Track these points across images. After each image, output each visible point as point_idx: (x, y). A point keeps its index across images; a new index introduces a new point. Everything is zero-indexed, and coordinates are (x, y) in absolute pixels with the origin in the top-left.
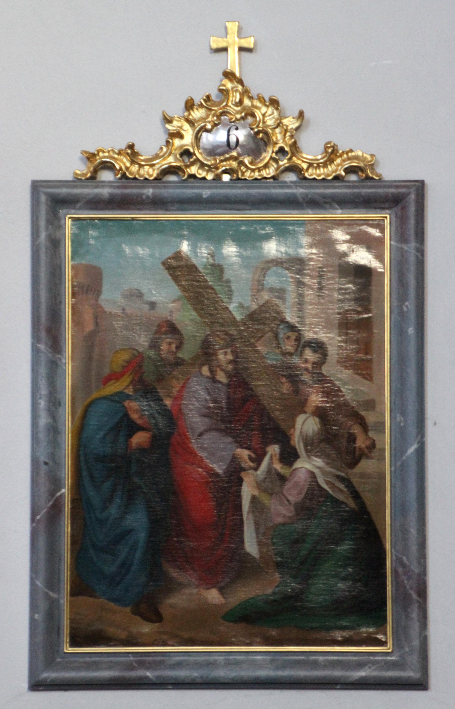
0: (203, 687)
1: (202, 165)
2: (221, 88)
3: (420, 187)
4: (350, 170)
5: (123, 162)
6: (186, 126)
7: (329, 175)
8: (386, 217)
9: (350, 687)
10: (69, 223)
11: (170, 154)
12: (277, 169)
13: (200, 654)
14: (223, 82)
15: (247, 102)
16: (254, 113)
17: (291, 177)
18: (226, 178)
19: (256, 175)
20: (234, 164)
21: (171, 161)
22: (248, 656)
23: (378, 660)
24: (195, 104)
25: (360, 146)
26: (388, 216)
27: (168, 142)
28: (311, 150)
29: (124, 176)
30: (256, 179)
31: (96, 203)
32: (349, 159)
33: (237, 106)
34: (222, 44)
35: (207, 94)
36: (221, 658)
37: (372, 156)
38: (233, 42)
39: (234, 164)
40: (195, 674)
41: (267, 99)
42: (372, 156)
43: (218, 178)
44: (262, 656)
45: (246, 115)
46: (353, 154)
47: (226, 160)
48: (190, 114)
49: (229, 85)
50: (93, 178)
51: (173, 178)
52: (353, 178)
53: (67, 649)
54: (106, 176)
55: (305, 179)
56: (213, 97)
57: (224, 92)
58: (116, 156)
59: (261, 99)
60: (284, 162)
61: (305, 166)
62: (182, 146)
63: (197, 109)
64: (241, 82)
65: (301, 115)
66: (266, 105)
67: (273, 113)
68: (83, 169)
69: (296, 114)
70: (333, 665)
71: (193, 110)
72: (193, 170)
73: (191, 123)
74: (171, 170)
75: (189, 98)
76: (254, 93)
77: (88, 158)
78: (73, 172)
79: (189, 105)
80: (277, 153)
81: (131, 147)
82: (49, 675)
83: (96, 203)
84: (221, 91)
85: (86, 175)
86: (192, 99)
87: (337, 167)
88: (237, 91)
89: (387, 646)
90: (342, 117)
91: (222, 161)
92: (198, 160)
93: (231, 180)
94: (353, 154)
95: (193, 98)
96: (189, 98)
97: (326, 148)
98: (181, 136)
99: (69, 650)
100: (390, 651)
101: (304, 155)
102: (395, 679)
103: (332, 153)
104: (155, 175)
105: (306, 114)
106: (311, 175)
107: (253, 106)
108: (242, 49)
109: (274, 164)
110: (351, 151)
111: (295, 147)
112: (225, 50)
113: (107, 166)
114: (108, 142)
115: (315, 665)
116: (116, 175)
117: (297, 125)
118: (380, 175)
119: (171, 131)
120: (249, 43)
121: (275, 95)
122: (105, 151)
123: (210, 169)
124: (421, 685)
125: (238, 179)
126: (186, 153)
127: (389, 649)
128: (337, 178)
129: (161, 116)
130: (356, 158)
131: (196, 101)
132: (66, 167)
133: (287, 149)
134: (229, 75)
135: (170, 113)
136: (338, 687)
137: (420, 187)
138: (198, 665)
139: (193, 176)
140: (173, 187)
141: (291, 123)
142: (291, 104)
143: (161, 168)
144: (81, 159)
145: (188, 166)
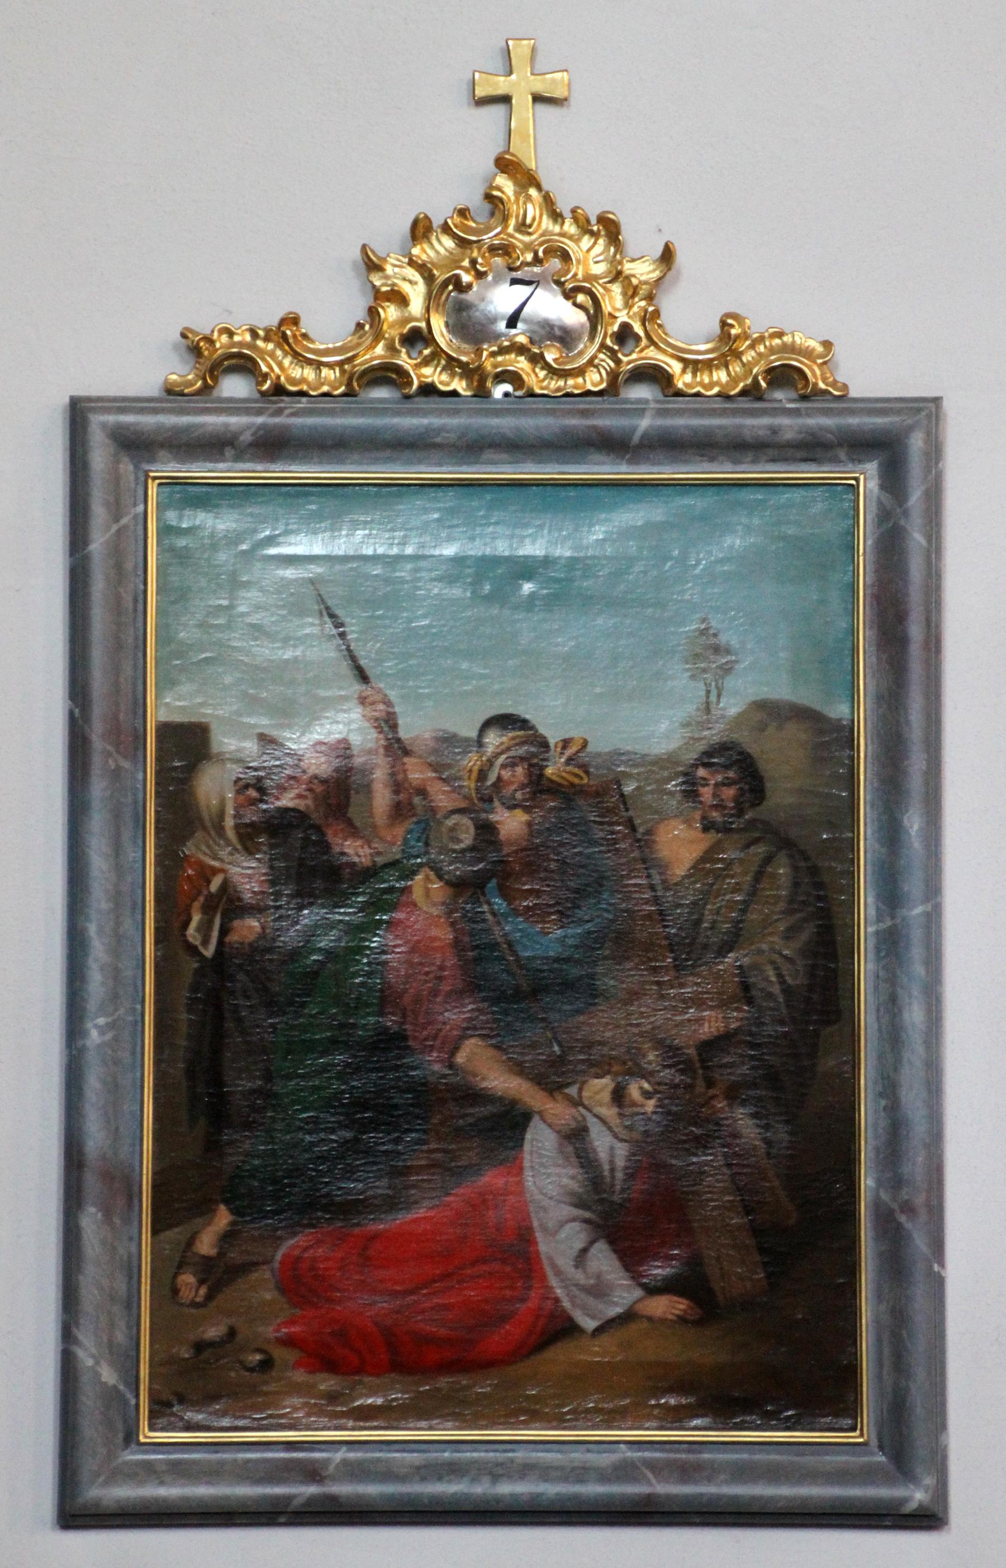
0: (632, 1520)
1: (452, 364)
2: (495, 193)
3: (928, 410)
4: (784, 376)
5: (282, 367)
8: (857, 479)
9: (730, 1519)
11: (378, 336)
13: (749, 1447)
17: (641, 392)
18: (499, 391)
20: (521, 364)
25: (793, 311)
27: (373, 312)
28: (688, 322)
29: (279, 390)
33: (530, 234)
34: (501, 85)
37: (827, 345)
38: (520, 85)
39: (521, 364)
40: (552, 1490)
41: (593, 220)
42: (827, 345)
43: (482, 393)
44: (779, 1453)
47: (502, 351)
49: (506, 186)
50: (206, 389)
51: (381, 393)
52: (779, 395)
53: (146, 1437)
54: (234, 387)
55: (679, 394)
57: (493, 201)
58: (260, 343)
59: (585, 228)
60: (631, 359)
61: (675, 367)
65: (667, 256)
66: (592, 233)
68: (180, 371)
70: (624, 1471)
72: (431, 374)
73: (423, 269)
74: (386, 374)
75: (422, 216)
76: (564, 206)
78: (161, 380)
79: (420, 230)
84: (489, 197)
85: (191, 384)
86: (426, 217)
90: (753, 257)
91: (493, 354)
92: (438, 353)
95: (430, 216)
97: (724, 324)
98: (401, 299)
100: (861, 1440)
102: (146, 1502)
103: (728, 341)
105: (682, 258)
110: (780, 335)
111: (649, 318)
112: (505, 99)
113: (243, 364)
114: (240, 311)
115: (313, 1473)
116: (261, 383)
117: (657, 274)
118: (845, 387)
120: (555, 83)
124: (929, 1519)
125: (532, 394)
126: (416, 338)
128: (752, 392)
129: (357, 254)
130: (792, 349)
132: (139, 366)
133: (638, 328)
134: (505, 164)
135: (379, 247)
136: (282, 1520)
137: (928, 410)
139: (428, 390)
140: (381, 410)
141: (643, 271)
143: (521, 372)
144: (176, 347)
145: (418, 366)
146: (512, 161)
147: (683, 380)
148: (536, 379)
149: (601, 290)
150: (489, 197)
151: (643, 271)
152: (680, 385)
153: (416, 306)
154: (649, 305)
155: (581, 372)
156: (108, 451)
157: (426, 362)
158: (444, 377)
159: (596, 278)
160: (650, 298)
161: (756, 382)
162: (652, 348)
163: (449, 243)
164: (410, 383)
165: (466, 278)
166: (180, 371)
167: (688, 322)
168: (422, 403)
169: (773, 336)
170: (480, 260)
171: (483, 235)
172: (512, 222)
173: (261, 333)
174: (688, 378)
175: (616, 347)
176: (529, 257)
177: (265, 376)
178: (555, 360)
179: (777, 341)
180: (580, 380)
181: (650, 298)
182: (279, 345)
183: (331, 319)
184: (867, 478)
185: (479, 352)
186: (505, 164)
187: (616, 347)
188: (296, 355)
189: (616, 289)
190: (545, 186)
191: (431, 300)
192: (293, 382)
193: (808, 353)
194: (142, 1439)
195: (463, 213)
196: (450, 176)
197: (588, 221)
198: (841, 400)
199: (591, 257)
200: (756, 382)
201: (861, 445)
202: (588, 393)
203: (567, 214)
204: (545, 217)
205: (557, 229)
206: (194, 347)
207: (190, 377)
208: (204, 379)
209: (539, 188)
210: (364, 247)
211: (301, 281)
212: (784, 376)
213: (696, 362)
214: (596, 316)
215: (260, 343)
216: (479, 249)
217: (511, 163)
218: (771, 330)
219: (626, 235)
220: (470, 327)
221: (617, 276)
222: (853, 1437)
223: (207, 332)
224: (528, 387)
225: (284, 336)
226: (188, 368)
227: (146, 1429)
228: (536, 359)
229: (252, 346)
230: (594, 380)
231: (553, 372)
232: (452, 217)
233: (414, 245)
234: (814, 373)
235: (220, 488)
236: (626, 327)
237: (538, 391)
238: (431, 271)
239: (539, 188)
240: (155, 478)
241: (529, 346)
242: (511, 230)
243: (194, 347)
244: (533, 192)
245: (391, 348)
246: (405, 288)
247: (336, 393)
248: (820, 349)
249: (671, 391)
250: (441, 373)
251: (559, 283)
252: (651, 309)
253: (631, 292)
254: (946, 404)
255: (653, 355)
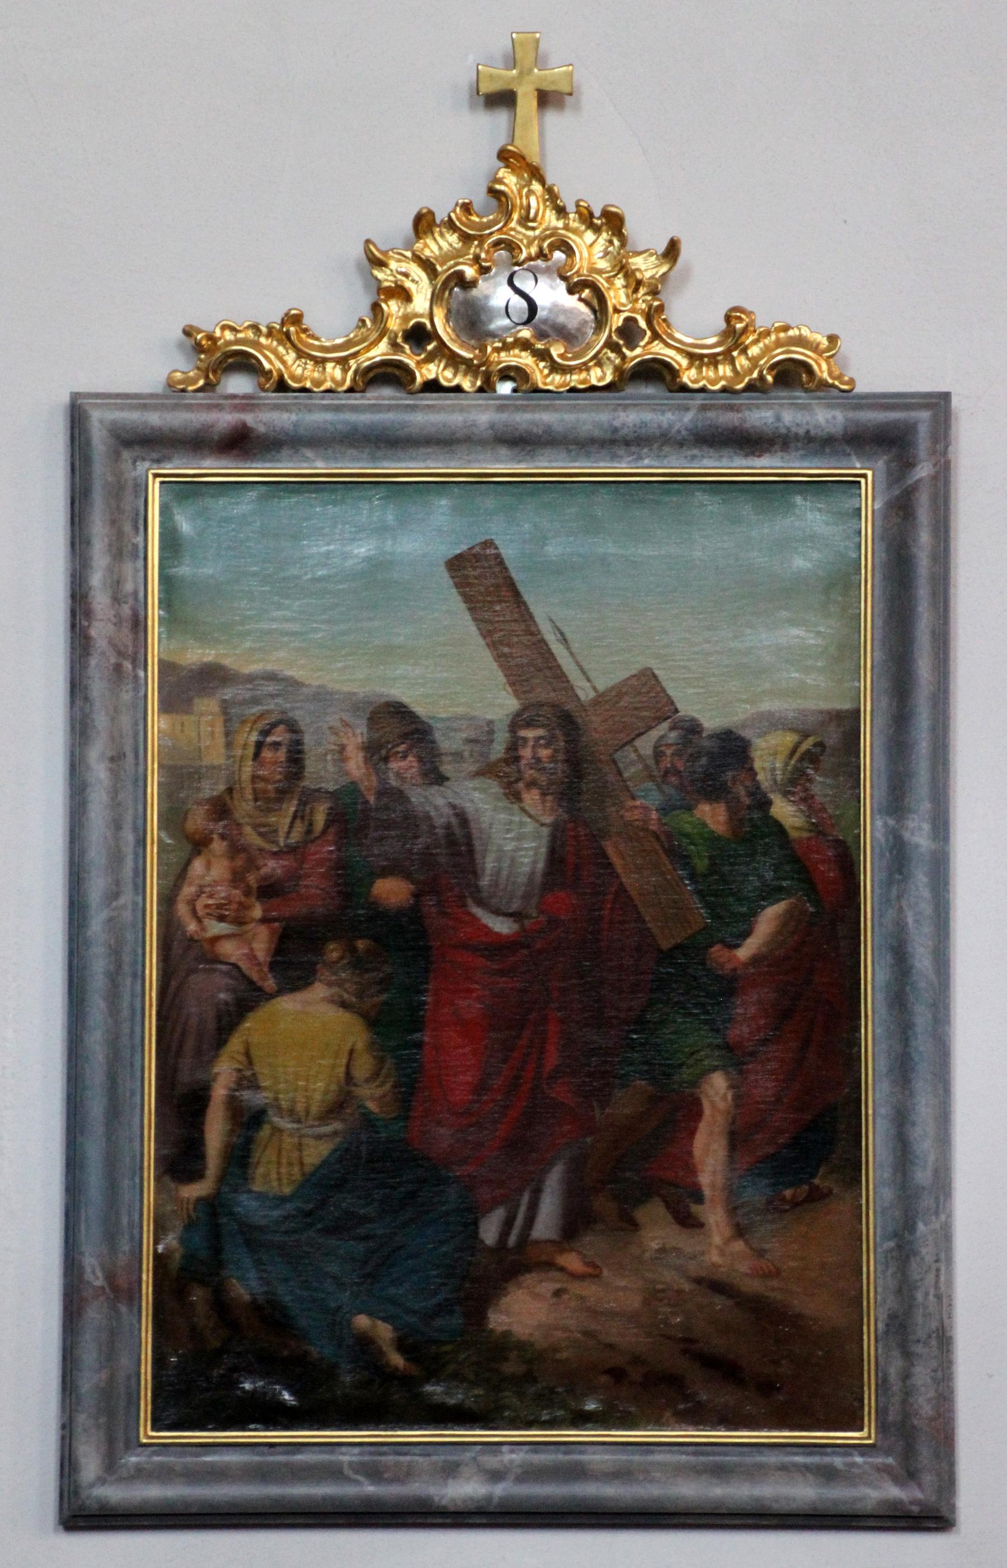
1: (454, 361)
2: (498, 187)
3: (939, 404)
4: (791, 375)
5: (279, 360)
6: (416, 271)
7: (713, 382)
8: (864, 476)
10: (154, 490)
12: (618, 370)
14: (500, 174)
15: (551, 219)
16: (568, 243)
18: (505, 388)
19: (574, 379)
20: (525, 359)
21: (380, 351)
22: (652, 1452)
23: (212, 1464)
24: (438, 221)
25: (800, 303)
26: (869, 473)
27: (376, 307)
28: (693, 321)
29: (282, 386)
30: (573, 390)
31: (197, 443)
32: (778, 344)
33: (533, 229)
35: (467, 201)
36: (345, 1458)
39: (525, 359)
41: (597, 213)
42: (832, 339)
43: (486, 388)
45: (553, 247)
46: (791, 333)
47: (506, 347)
48: (426, 245)
49: (510, 182)
51: (386, 393)
54: (238, 384)
55: (684, 389)
56: (476, 206)
58: (263, 340)
59: (587, 218)
60: (635, 354)
62: (406, 318)
63: (442, 235)
64: (536, 173)
65: (672, 251)
67: (611, 242)
69: (662, 247)
70: (530, 1474)
71: (433, 234)
72: (431, 371)
73: (428, 266)
74: (389, 375)
76: (568, 201)
77: (198, 348)
79: (423, 223)
80: (621, 331)
81: (296, 319)
82: (115, 1494)
83: (197, 443)
84: (492, 192)
87: (758, 355)
88: (530, 192)
89: (861, 1429)
90: (769, 247)
91: (498, 350)
93: (515, 390)
94: (791, 333)
96: (425, 211)
97: (728, 318)
98: (405, 296)
99: (147, 1434)
100: (871, 1442)
101: (678, 335)
103: (734, 333)
104: (348, 383)
106: (693, 382)
107: (566, 227)
108: (545, 99)
109: (612, 355)
110: (786, 328)
113: (243, 363)
114: (237, 305)
115: (334, 1473)
118: (852, 382)
119: (386, 284)
121: (616, 204)
122: (238, 328)
123: (469, 367)
124: (933, 1518)
125: (537, 390)
126: (418, 335)
127: (869, 1437)
129: (358, 251)
130: (801, 341)
131: (440, 216)
132: (139, 363)
137: (939, 404)
138: (262, 1474)
139: (433, 386)
142: (647, 232)
144: (180, 346)
146: (514, 152)
147: (689, 377)
148: (540, 374)
149: (606, 285)
150: (492, 192)
151: (646, 267)
152: (685, 379)
153: (421, 302)
154: (654, 300)
155: (585, 367)
156: (104, 453)
157: (430, 358)
158: (449, 373)
159: (600, 272)
160: (654, 293)
161: (762, 378)
162: (656, 342)
163: (453, 238)
164: (414, 379)
165: (470, 272)
166: (182, 366)
167: (693, 321)
168: (431, 399)
169: (779, 330)
170: (483, 255)
171: (488, 227)
172: (515, 216)
173: (264, 330)
174: (693, 372)
175: (621, 342)
176: (534, 250)
177: (270, 371)
178: (561, 356)
179: (782, 335)
180: (583, 375)
181: (654, 293)
182: (280, 342)
183: (334, 314)
184: (869, 475)
185: (483, 349)
186: (504, 156)
187: (621, 342)
188: (301, 354)
189: (620, 282)
190: (549, 182)
191: (436, 298)
192: (293, 378)
193: (815, 348)
194: (145, 1441)
195: (467, 208)
196: (453, 160)
197: (591, 215)
198: (846, 397)
199: (592, 250)
200: (762, 378)
201: (860, 440)
202: (593, 389)
203: (571, 208)
204: (548, 212)
205: (560, 224)
206: (198, 344)
207: (191, 374)
208: (207, 377)
209: (542, 181)
210: (368, 242)
211: (298, 269)
212: (791, 375)
213: (702, 356)
214: (599, 305)
215: (263, 340)
216: (481, 245)
217: (514, 155)
218: (777, 325)
219: (629, 228)
220: (472, 321)
221: (623, 268)
222: (852, 1436)
223: (210, 329)
224: (532, 384)
225: (288, 335)
226: (191, 366)
227: (149, 1427)
228: (543, 355)
229: (256, 345)
230: (599, 376)
231: (555, 368)
232: (454, 211)
233: (417, 242)
234: (822, 370)
235: (189, 485)
236: (630, 321)
237: (541, 386)
238: (434, 265)
239: (542, 181)
240: (156, 476)
241: (532, 341)
242: (513, 224)
243: (198, 344)
244: (536, 186)
245: (394, 345)
246: (408, 284)
247: (340, 389)
248: (825, 343)
249: (676, 387)
250: (444, 369)
251: (564, 278)
252: (656, 303)
253: (635, 284)
254: (955, 401)
255: (658, 349)
